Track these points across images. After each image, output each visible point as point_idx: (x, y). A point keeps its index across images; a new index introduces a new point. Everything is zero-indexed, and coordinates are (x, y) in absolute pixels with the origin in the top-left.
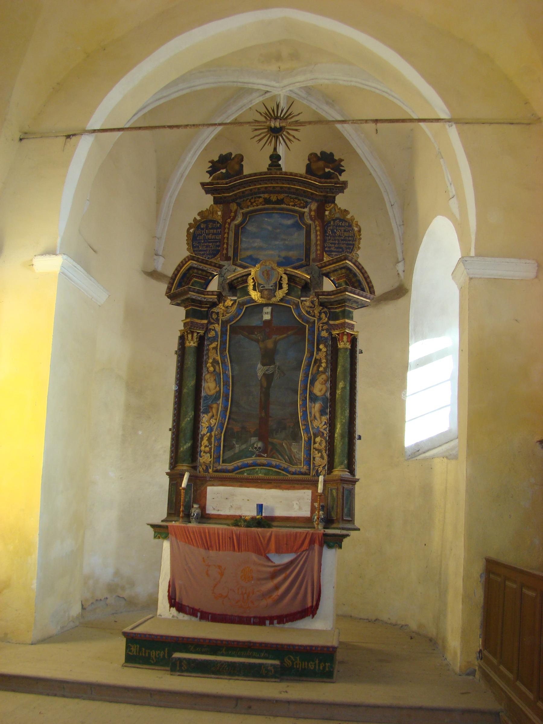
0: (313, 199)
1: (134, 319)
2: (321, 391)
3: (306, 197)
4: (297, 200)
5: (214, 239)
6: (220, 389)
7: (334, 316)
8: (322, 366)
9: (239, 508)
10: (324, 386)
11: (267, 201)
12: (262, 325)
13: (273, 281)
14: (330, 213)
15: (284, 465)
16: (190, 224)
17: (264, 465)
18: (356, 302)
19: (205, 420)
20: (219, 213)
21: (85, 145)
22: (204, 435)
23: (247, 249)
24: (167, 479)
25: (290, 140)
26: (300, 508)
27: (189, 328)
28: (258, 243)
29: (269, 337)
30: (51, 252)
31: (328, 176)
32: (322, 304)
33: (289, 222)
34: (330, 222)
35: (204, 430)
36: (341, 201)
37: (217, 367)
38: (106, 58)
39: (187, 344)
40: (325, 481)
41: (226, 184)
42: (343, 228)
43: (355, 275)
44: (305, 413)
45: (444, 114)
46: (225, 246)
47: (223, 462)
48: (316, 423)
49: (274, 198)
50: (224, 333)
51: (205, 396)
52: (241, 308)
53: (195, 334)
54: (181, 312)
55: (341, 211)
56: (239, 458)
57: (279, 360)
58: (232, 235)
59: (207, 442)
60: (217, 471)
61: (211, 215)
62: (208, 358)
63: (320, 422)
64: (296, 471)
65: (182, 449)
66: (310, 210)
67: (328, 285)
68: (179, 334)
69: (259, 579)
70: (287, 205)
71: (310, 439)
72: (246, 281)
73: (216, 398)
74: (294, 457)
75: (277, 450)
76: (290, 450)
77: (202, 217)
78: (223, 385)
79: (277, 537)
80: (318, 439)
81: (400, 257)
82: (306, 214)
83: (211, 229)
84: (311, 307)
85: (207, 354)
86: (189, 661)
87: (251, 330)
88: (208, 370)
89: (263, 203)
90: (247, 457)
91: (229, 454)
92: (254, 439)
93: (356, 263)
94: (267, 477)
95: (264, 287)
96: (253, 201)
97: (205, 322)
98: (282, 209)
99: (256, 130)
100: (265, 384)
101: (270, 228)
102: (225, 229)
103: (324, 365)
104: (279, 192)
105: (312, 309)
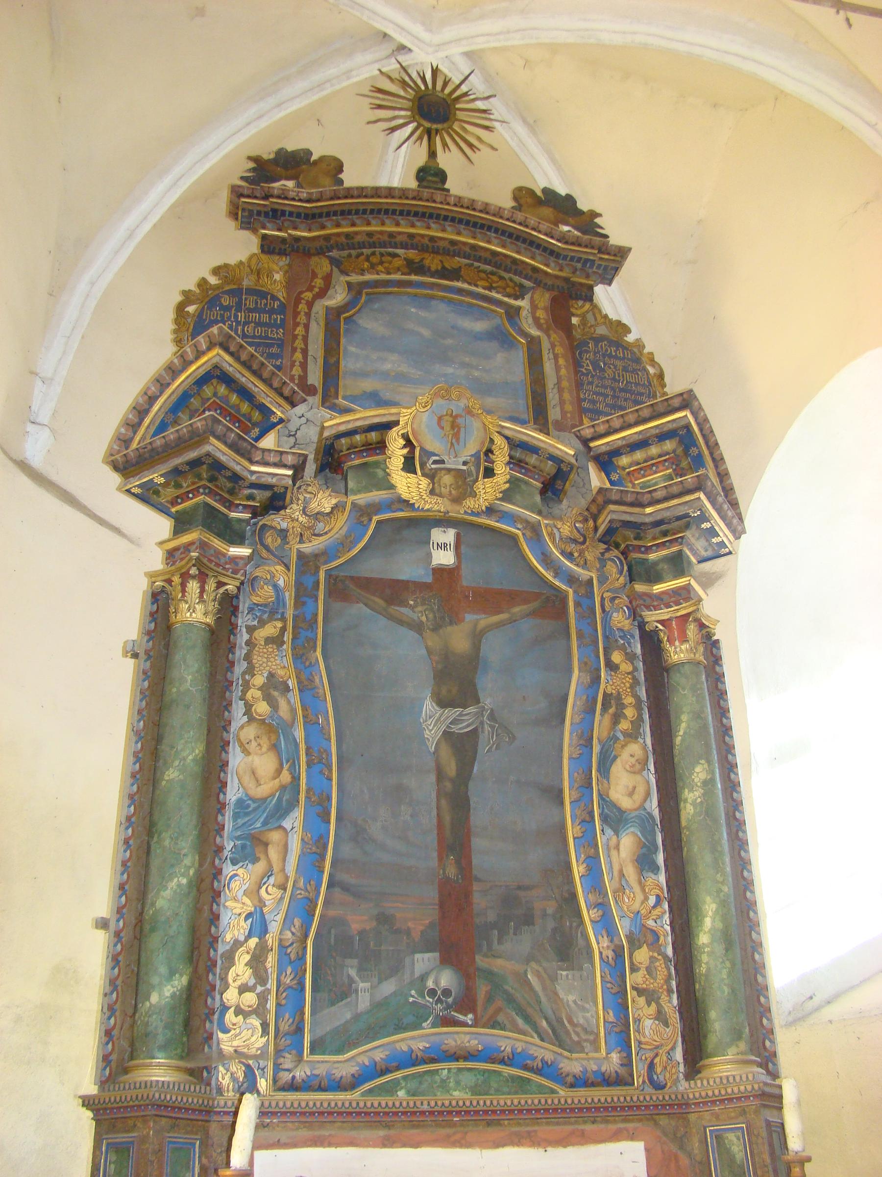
0: (538, 283)
2: (631, 794)
3: (519, 274)
4: (495, 278)
5: (260, 337)
6: (296, 779)
8: (625, 717)
10: (638, 777)
12: (429, 579)
14: (584, 321)
15: (543, 1051)
16: (186, 294)
17: (469, 1056)
19: (239, 883)
23: (364, 375)
24: (82, 1127)
25: (471, 146)
27: (185, 566)
28: (391, 363)
29: (455, 619)
33: (480, 326)
35: (233, 924)
36: (610, 299)
37: (283, 704)
41: (308, 201)
42: (619, 363)
46: (298, 356)
47: (313, 1051)
48: (634, 900)
51: (240, 802)
52: (365, 519)
53: (211, 585)
55: (610, 321)
56: (372, 1033)
57: (490, 690)
58: (317, 332)
59: (249, 971)
60: (293, 1086)
61: (253, 278)
62: (251, 670)
63: (640, 897)
64: (585, 1071)
65: (154, 998)
66: (534, 307)
70: (470, 284)
71: (618, 952)
72: (381, 446)
74: (570, 1021)
75: (510, 1000)
77: (226, 280)
78: (309, 764)
80: (642, 955)
82: (524, 313)
83: (250, 310)
84: (575, 541)
87: (393, 592)
88: (248, 711)
89: (406, 270)
90: (400, 1028)
91: (341, 1015)
92: (423, 961)
95: (443, 462)
96: (374, 260)
99: (380, 107)
100: (451, 769)
101: (426, 333)
102: (296, 314)
104: (446, 252)
105: (579, 547)
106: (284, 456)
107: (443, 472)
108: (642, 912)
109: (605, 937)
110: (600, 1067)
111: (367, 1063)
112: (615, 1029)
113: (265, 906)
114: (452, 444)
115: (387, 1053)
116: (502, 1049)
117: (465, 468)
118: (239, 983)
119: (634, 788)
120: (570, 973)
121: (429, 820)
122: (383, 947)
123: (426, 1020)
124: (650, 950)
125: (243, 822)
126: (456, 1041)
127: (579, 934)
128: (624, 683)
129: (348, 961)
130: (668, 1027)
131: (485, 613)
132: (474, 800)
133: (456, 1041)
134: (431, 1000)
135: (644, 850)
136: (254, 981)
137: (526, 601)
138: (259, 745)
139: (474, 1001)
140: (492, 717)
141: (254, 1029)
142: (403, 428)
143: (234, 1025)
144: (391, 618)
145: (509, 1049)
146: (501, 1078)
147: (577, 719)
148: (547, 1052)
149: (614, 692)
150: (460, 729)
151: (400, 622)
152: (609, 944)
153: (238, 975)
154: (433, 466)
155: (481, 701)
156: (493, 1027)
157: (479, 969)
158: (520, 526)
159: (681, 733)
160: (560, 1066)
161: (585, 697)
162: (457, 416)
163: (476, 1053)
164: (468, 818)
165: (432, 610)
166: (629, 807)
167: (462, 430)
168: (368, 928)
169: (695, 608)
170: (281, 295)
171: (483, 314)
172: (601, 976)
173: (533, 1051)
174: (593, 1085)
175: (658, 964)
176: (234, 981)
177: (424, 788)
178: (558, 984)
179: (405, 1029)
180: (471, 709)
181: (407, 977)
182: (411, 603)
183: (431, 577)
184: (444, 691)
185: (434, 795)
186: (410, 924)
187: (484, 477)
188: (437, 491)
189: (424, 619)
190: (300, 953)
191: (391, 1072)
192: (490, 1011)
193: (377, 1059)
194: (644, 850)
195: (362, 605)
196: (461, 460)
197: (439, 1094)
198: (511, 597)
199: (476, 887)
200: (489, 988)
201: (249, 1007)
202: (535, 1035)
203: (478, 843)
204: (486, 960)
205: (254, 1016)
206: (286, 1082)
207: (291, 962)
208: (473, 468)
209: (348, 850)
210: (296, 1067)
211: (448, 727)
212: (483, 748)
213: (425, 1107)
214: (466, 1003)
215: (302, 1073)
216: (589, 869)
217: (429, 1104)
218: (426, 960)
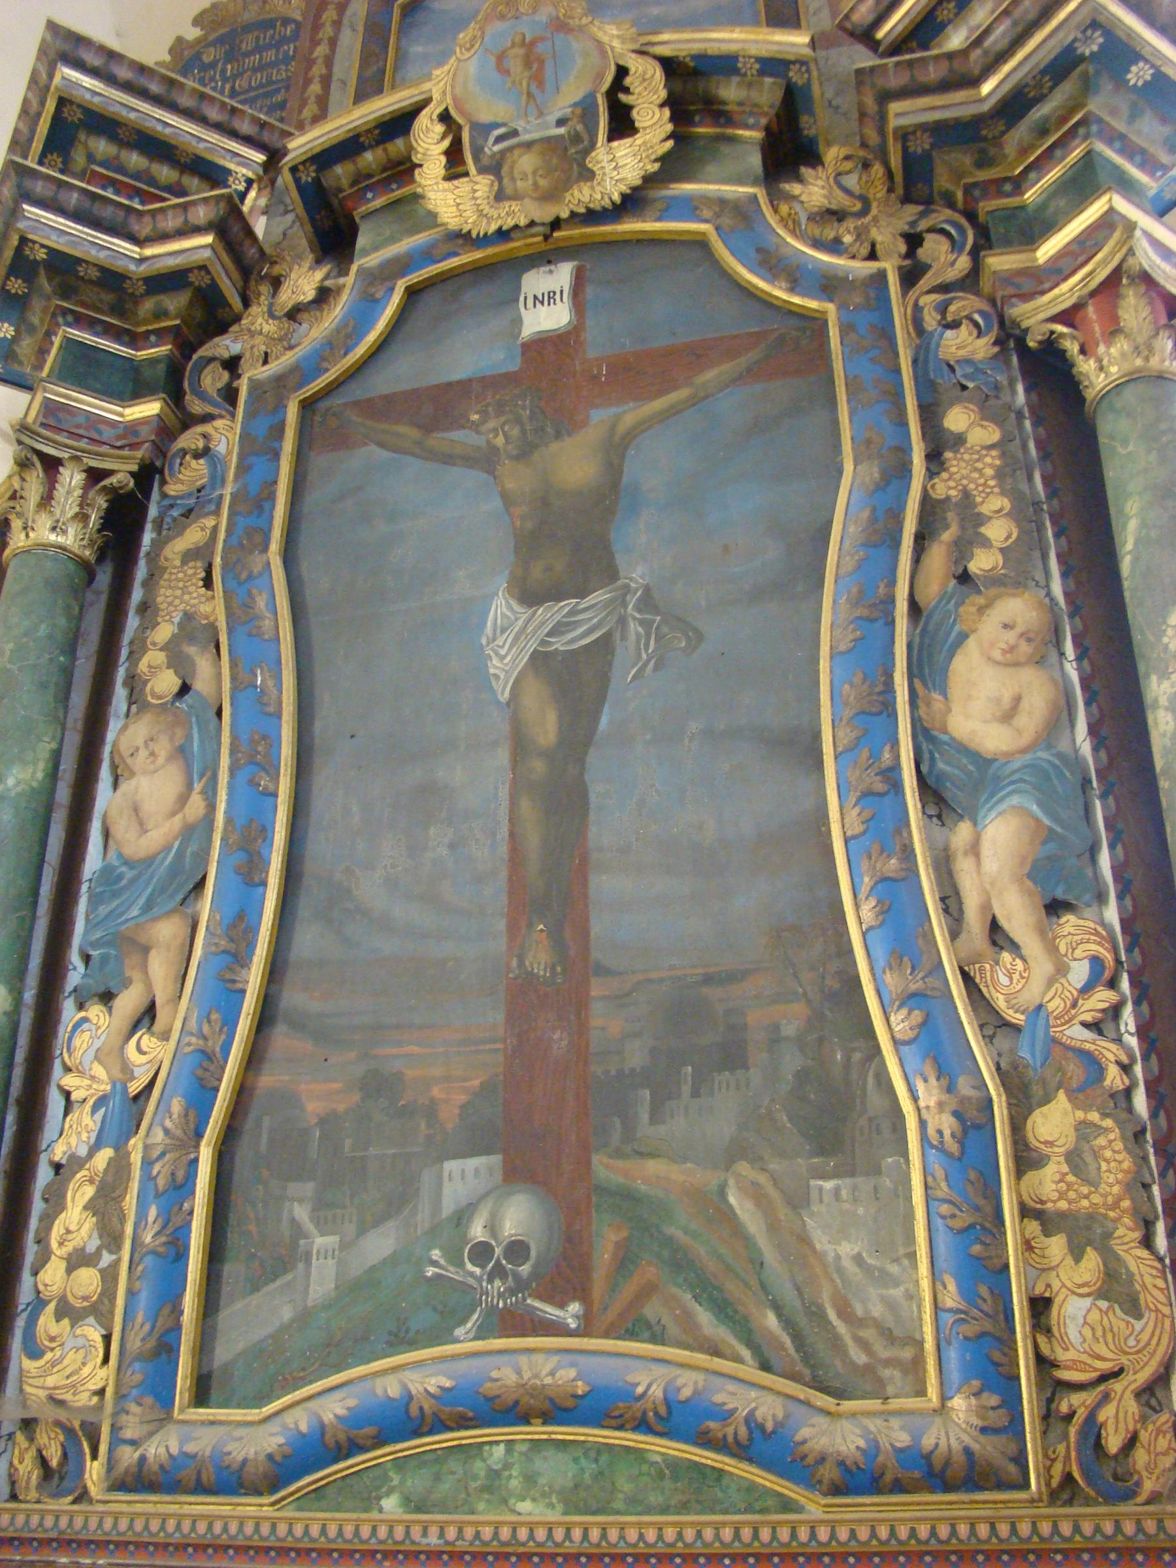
2: (1008, 716)
8: (986, 543)
15: (752, 1396)
17: (556, 1410)
29: (564, 423)
44: (896, 893)
56: (335, 1352)
63: (1042, 967)
71: (974, 1122)
74: (845, 1313)
75: (680, 1262)
80: (1053, 1123)
87: (441, 405)
92: (463, 1176)
100: (546, 727)
103: (998, 531)
106: (192, 210)
107: (516, 152)
108: (1051, 1006)
109: (933, 1080)
110: (916, 1438)
111: (304, 1427)
112: (963, 1328)
113: (133, 1078)
114: (529, 95)
115: (352, 1403)
116: (640, 1390)
117: (562, 130)
118: (69, 1247)
119: (1017, 699)
120: (845, 1183)
121: (489, 852)
122: (373, 1151)
123: (463, 1321)
124: (1076, 1105)
125: (108, 909)
126: (519, 1373)
127: (870, 1080)
128: (980, 471)
129: (293, 1188)
130: (1139, 1316)
131: (636, 399)
132: (596, 790)
133: (519, 1373)
134: (478, 1271)
135: (1052, 847)
136: (98, 1242)
137: (732, 354)
138: (152, 754)
139: (585, 1269)
140: (648, 602)
141: (89, 1347)
142: (440, 103)
143: (52, 1339)
144: (432, 456)
145: (657, 1392)
146: (645, 1468)
147: (849, 564)
148: (770, 1398)
149: (953, 493)
150: (573, 641)
151: (448, 459)
152: (945, 1097)
153: (68, 1232)
154: (496, 148)
155: (622, 574)
156: (631, 1335)
157: (601, 1190)
158: (707, 214)
159: (1129, 546)
160: (798, 1438)
161: (866, 514)
162: (533, 43)
163: (570, 1403)
164: (582, 832)
165: (518, 421)
166: (1004, 748)
167: (549, 65)
168: (341, 1108)
169: (1124, 250)
172: (926, 1187)
173: (727, 1396)
174: (898, 1487)
175: (1101, 1141)
176: (61, 1244)
177: (483, 783)
178: (812, 1215)
179: (412, 1344)
180: (599, 597)
181: (423, 1218)
182: (475, 417)
183: (519, 360)
184: (537, 571)
185: (504, 793)
186: (436, 1092)
187: (611, 139)
188: (509, 191)
189: (500, 441)
190: (180, 1174)
191: (364, 1449)
192: (628, 1290)
193: (328, 1417)
194: (1052, 847)
195: (373, 447)
196: (552, 118)
197: (481, 1506)
198: (696, 355)
199: (597, 988)
200: (625, 1234)
201: (85, 1298)
202: (746, 1353)
204: (619, 1163)
205: (91, 1320)
206: (126, 1472)
207: (158, 1195)
208: (580, 127)
210: (151, 1434)
211: (543, 643)
212: (624, 671)
213: (433, 1540)
214: (566, 1274)
215: (162, 1450)
216: (885, 910)
217: (442, 1535)
218: (470, 1174)
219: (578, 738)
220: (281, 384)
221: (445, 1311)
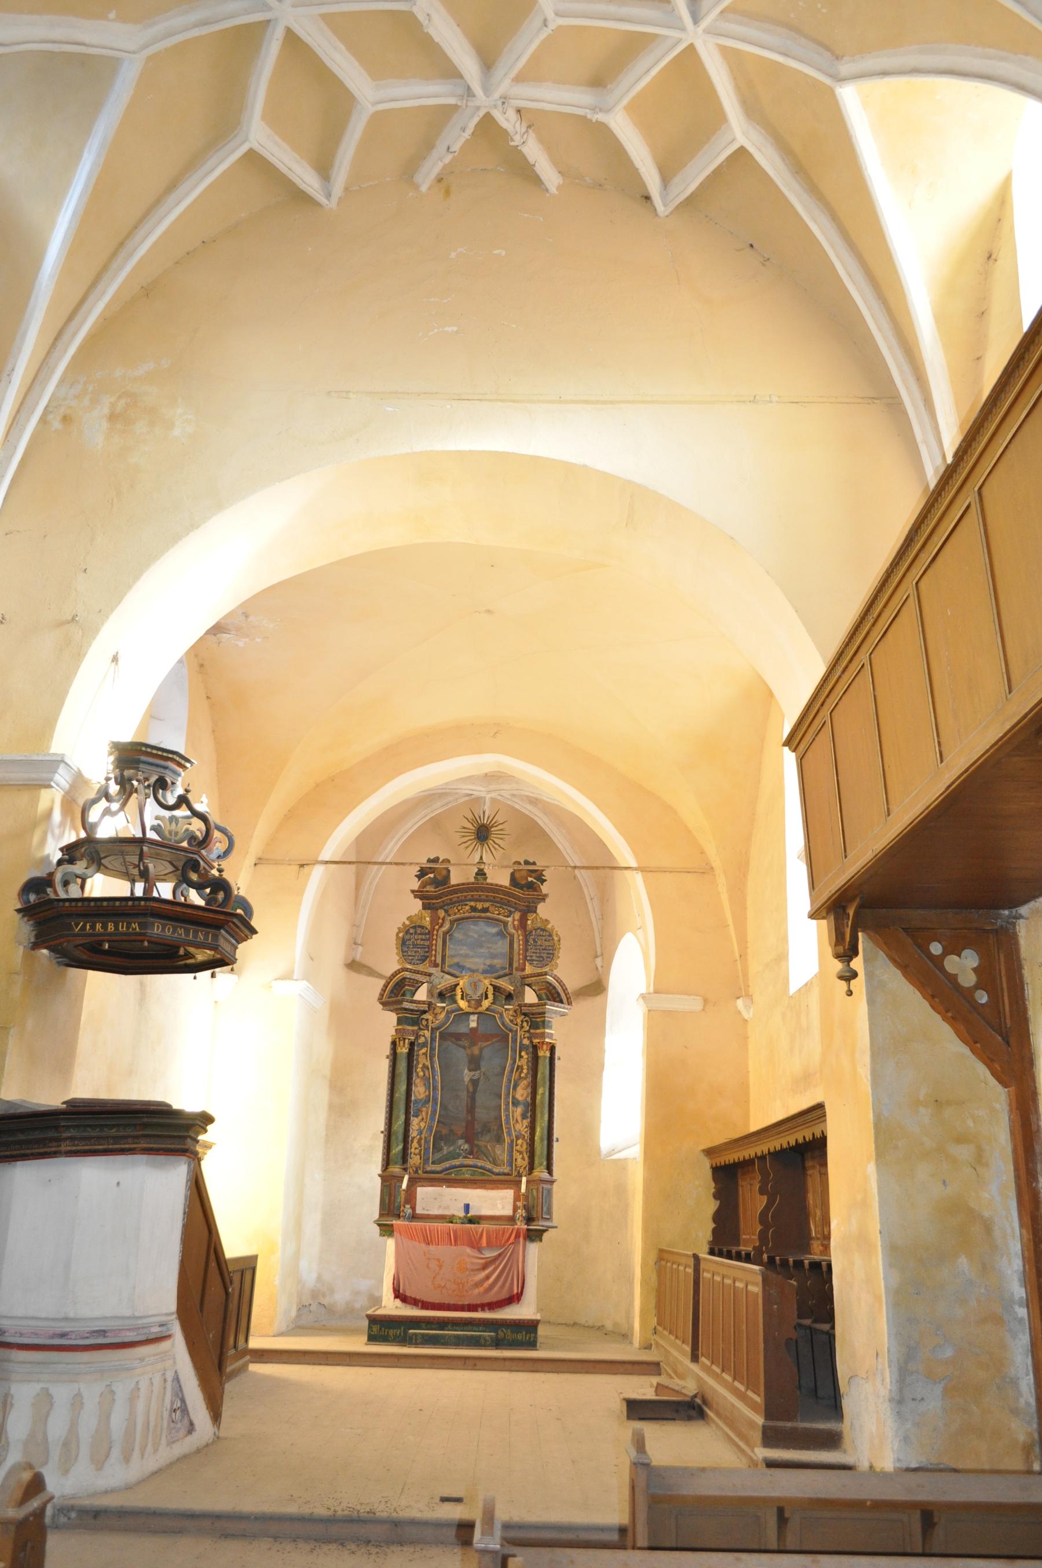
0: (516, 909)
1: (340, 1019)
7: (534, 1025)
9: (448, 1208)
11: (474, 909)
13: (479, 994)
15: (489, 1166)
18: (556, 1012)
19: (415, 1122)
20: (428, 919)
21: (317, 873)
22: (413, 1138)
24: (379, 1180)
26: (503, 1208)
28: (464, 950)
30: (288, 976)
31: (531, 886)
32: (525, 1014)
33: (494, 930)
34: (531, 932)
35: (413, 1133)
36: (541, 908)
38: (330, 793)
39: (399, 1050)
40: (528, 1182)
43: (554, 988)
44: (507, 1116)
45: (633, 864)
48: (518, 1126)
49: (479, 906)
50: (433, 1039)
54: (392, 1018)
56: (447, 1160)
57: (484, 1066)
62: (418, 1063)
66: (514, 920)
67: (530, 997)
68: (390, 1040)
69: (473, 1270)
71: (512, 1141)
73: (427, 1101)
75: (482, 1152)
76: (494, 1151)
77: (411, 922)
79: (488, 1232)
80: (520, 1142)
81: (599, 953)
85: (417, 1060)
86: (423, 1335)
87: (457, 1037)
91: (438, 1155)
92: (460, 1142)
93: (555, 977)
94: (473, 1178)
97: (416, 1028)
98: (488, 918)
100: (471, 1089)
101: (476, 936)
103: (525, 1071)
104: (484, 901)
170: (429, 927)
171: (497, 925)
177: (464, 1095)
203: (477, 1110)
209: (443, 1113)
212: (481, 1083)
219: (475, 1091)
220: (438, 1028)
221: (458, 1156)
